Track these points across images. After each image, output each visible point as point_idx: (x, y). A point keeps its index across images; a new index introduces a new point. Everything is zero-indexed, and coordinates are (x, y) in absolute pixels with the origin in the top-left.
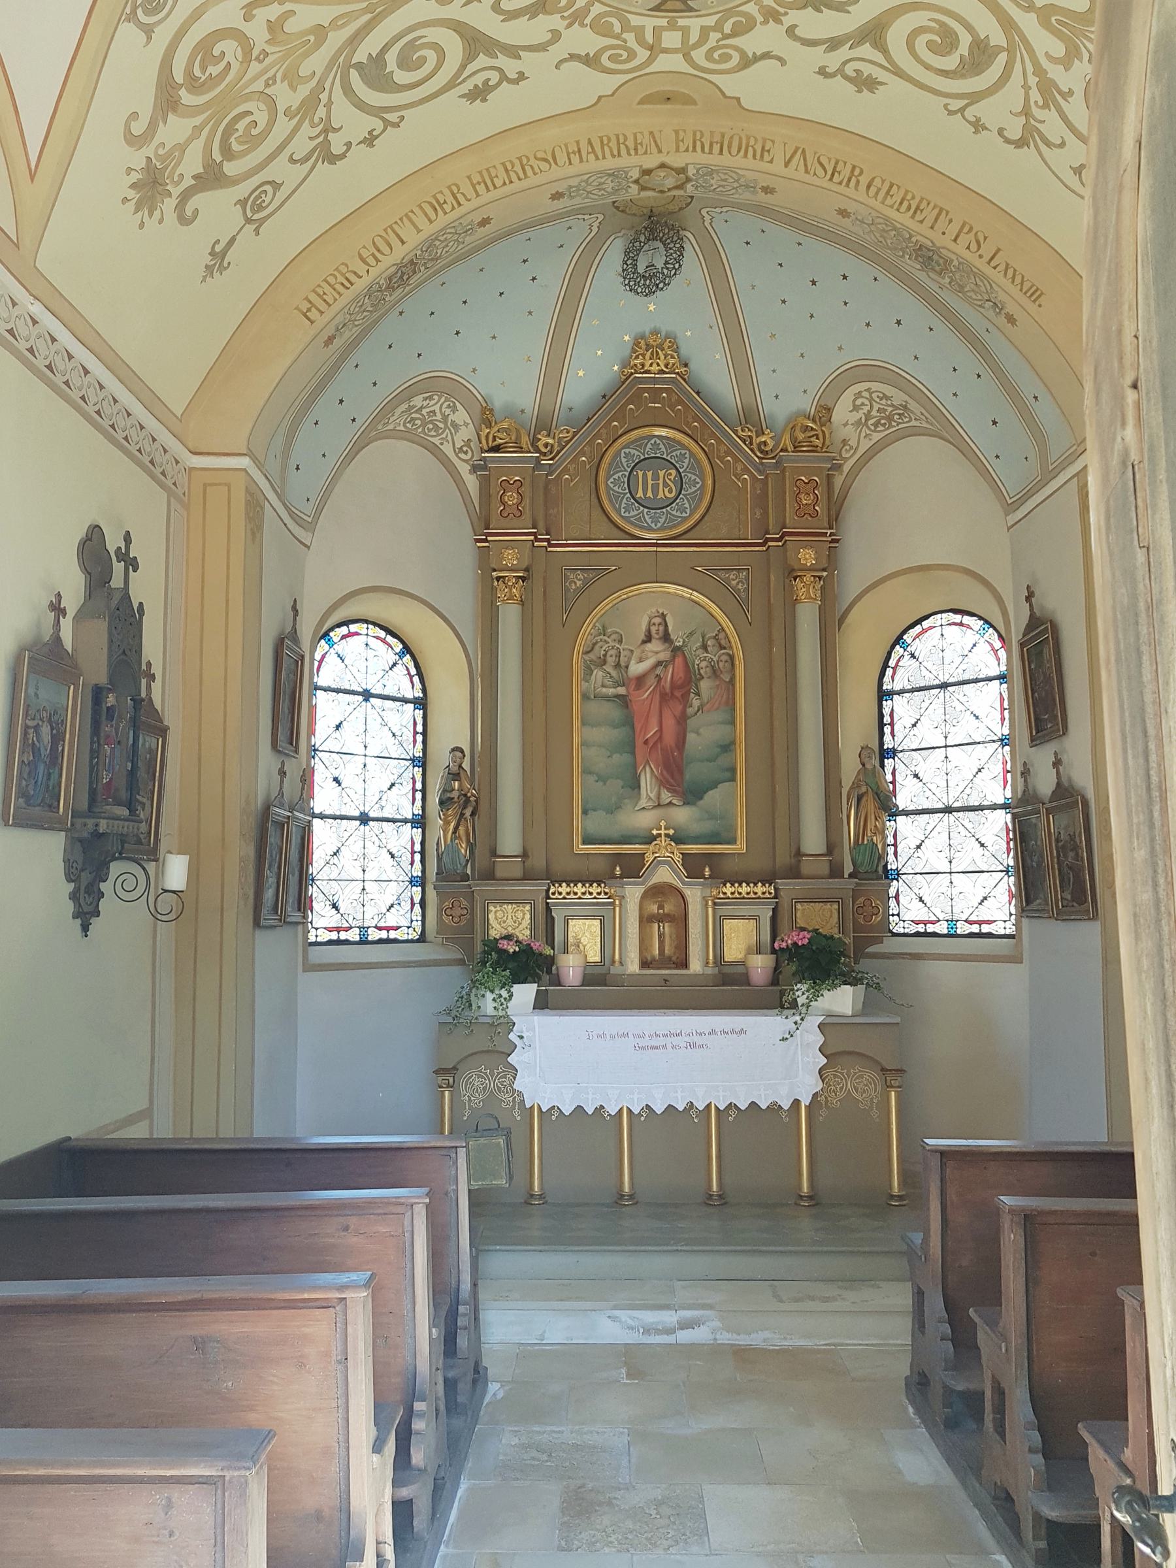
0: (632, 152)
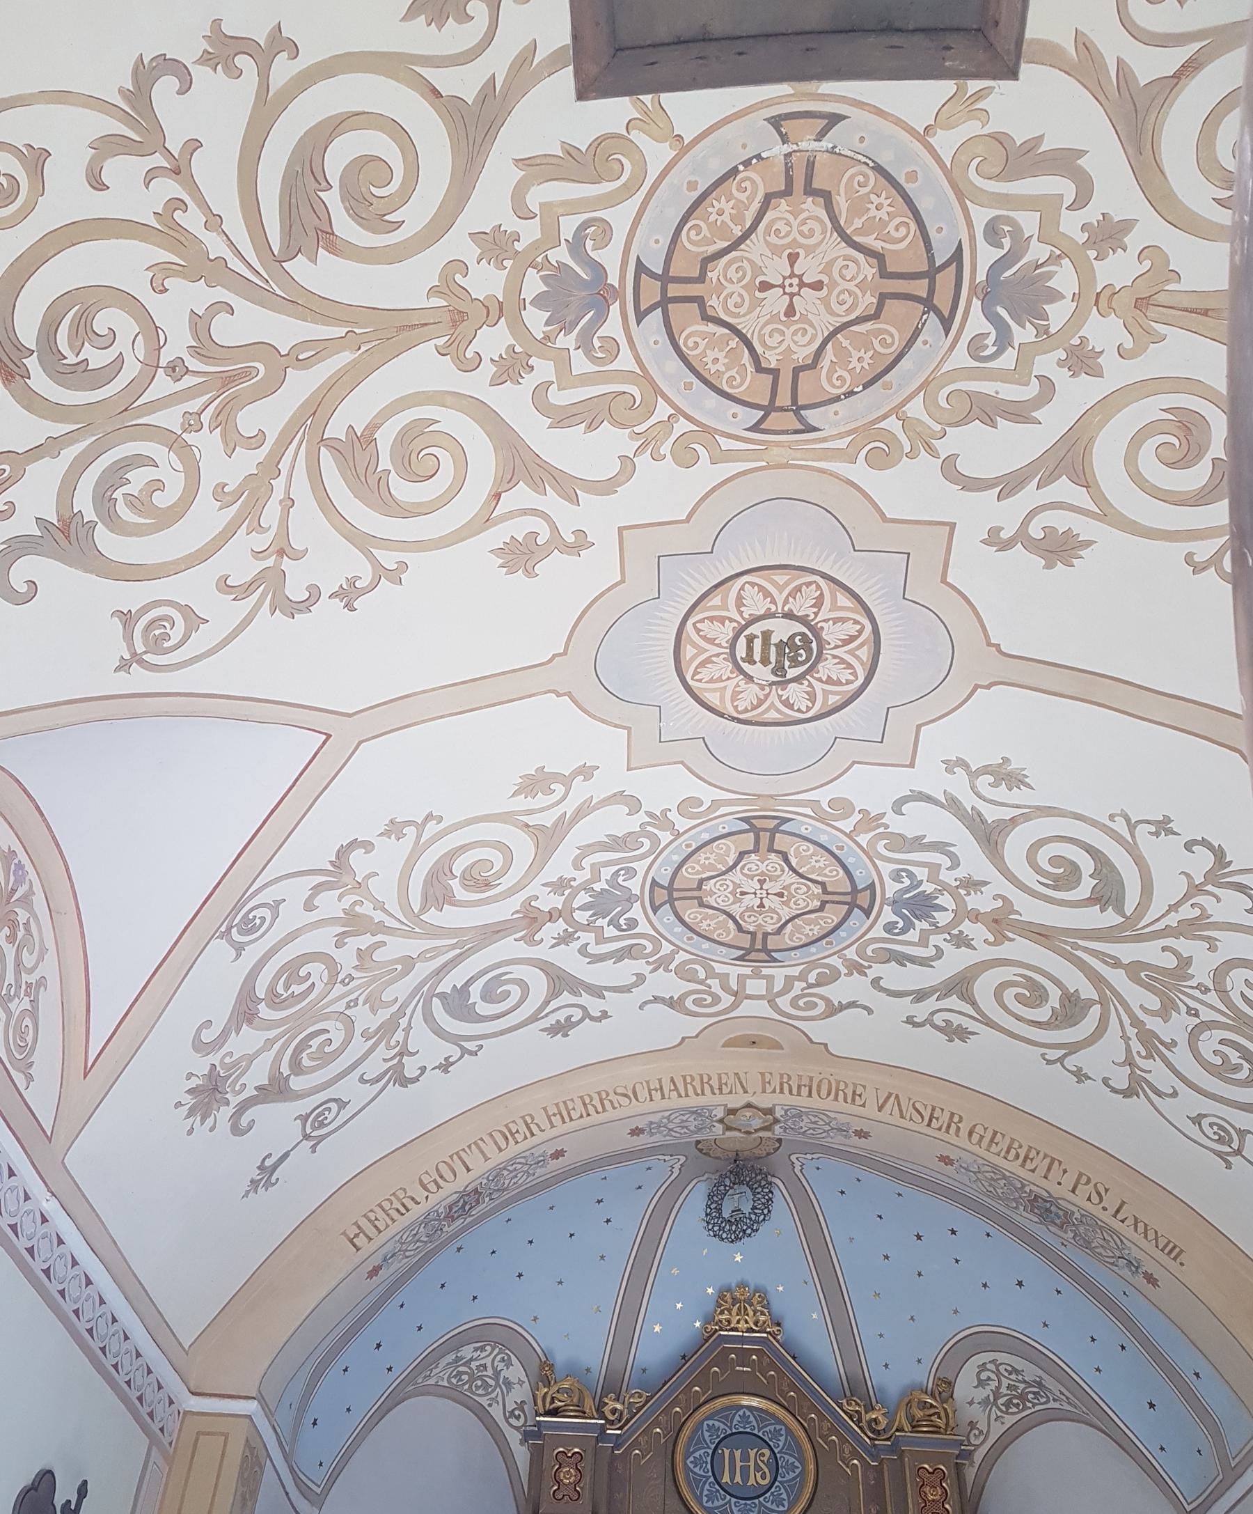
0: (717, 1091)
